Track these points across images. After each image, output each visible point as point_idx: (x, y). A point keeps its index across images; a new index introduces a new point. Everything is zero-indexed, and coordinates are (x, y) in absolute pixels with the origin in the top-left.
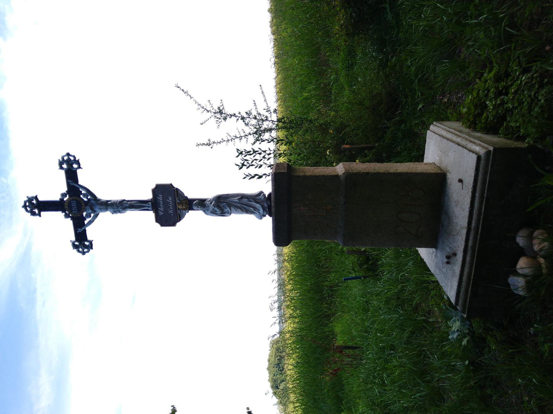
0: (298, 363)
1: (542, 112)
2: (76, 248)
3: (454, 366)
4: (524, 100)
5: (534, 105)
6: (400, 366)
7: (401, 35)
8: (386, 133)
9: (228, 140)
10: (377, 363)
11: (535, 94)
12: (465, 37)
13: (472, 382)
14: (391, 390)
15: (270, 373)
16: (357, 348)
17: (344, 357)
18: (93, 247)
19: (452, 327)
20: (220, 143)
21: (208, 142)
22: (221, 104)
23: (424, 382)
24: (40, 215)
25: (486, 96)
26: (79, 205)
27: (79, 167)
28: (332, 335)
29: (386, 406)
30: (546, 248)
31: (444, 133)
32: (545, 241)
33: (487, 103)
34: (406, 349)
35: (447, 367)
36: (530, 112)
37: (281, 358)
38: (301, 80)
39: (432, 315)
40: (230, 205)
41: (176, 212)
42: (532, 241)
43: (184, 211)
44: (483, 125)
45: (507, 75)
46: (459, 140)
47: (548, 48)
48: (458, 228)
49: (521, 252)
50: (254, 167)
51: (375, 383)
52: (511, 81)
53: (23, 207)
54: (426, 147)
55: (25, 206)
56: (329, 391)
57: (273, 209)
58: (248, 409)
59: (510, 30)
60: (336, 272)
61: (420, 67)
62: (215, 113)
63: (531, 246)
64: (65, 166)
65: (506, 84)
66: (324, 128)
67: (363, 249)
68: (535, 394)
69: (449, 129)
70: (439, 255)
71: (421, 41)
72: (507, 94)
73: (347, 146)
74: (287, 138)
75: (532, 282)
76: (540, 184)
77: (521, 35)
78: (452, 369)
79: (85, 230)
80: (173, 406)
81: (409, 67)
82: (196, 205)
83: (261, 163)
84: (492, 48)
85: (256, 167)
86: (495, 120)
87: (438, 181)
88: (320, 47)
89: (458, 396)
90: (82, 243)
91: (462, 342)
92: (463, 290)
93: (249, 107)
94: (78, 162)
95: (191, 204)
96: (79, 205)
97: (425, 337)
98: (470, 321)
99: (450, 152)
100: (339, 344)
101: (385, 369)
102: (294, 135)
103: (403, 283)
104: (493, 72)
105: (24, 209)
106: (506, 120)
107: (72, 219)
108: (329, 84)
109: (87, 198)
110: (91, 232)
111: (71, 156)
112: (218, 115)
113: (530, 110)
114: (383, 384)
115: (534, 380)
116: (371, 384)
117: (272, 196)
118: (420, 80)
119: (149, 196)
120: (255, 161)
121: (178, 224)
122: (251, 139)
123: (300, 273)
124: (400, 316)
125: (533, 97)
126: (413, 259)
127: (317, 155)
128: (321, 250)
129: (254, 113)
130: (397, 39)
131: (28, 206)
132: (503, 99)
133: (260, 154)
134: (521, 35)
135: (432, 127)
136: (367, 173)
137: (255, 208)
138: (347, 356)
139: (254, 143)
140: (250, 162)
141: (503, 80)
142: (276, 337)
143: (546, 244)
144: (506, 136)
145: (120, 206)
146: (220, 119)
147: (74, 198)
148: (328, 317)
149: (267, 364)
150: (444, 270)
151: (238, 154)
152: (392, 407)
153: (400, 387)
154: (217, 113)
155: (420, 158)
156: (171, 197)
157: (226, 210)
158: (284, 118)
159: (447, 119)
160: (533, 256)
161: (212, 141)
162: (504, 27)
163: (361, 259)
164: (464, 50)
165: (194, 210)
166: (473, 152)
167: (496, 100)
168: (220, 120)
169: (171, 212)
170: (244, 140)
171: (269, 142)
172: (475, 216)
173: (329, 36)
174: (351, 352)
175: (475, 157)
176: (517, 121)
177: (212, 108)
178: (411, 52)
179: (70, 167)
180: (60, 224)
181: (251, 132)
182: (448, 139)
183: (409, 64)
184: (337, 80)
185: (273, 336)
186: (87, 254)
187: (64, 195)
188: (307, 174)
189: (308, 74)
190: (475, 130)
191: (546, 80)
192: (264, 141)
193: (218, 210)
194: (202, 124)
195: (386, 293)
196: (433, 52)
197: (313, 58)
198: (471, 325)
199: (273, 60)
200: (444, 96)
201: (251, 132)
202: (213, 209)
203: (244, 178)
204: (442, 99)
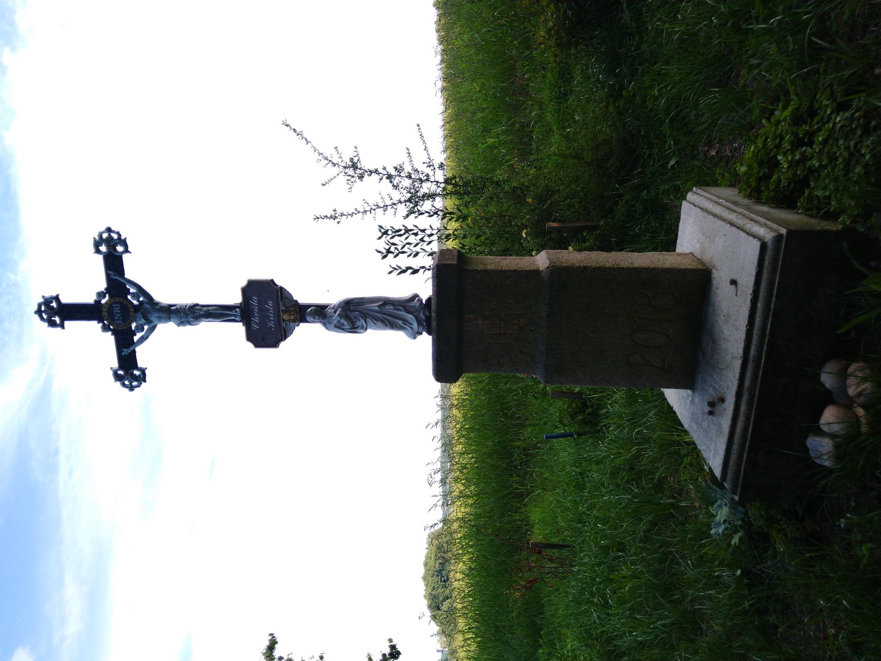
0: (470, 569)
1: (866, 173)
2: (119, 380)
3: (718, 577)
4: (838, 154)
5: (853, 162)
6: (634, 576)
7: (644, 47)
9: (365, 212)
10: (596, 572)
11: (856, 145)
12: (747, 51)
13: (746, 604)
14: (618, 614)
15: (427, 586)
16: (565, 546)
19: (715, 516)
20: (352, 215)
22: (355, 154)
24: (63, 327)
25: (778, 147)
26: (124, 311)
27: (126, 251)
28: (526, 525)
31: (709, 206)
32: (866, 381)
33: (780, 158)
35: (708, 579)
36: (846, 174)
37: (445, 562)
38: (483, 117)
43: (292, 324)
44: (772, 194)
46: (732, 217)
48: (729, 358)
49: (827, 398)
50: (406, 255)
51: (592, 603)
52: (817, 123)
53: (36, 312)
54: (681, 228)
55: (39, 312)
56: (519, 614)
57: (434, 324)
58: (390, 640)
59: (819, 42)
60: (535, 425)
61: (673, 98)
62: (345, 167)
63: (844, 388)
64: (103, 248)
65: (810, 127)
66: (518, 195)
67: (577, 390)
68: (846, 624)
70: (697, 400)
72: (810, 144)
73: (554, 225)
74: (459, 210)
75: (845, 445)
78: (716, 583)
79: (134, 352)
80: (271, 635)
81: (656, 99)
82: (311, 314)
83: (418, 249)
84: (788, 70)
86: (792, 186)
87: (698, 281)
90: (129, 371)
92: (733, 457)
93: (400, 158)
94: (124, 243)
95: (303, 313)
96: (124, 311)
98: (744, 507)
99: (718, 236)
101: (608, 581)
103: (639, 444)
104: (790, 109)
105: (37, 317)
106: (808, 186)
107: (115, 333)
108: (528, 125)
109: (138, 301)
110: (144, 355)
111: (114, 232)
112: (351, 172)
113: (847, 170)
115: (845, 602)
116: (585, 604)
117: (433, 302)
118: (672, 120)
119: (235, 298)
120: (407, 246)
121: (282, 344)
122: (403, 209)
123: (477, 427)
124: (634, 497)
125: (852, 150)
129: (408, 168)
130: (638, 54)
131: (44, 311)
132: (805, 152)
133: (416, 234)
135: (690, 196)
136: (585, 267)
137: (405, 321)
138: (549, 559)
139: (407, 216)
140: (399, 247)
141: (805, 122)
143: (867, 385)
144: (807, 211)
146: (353, 177)
147: (117, 299)
148: (520, 496)
149: (422, 571)
151: (380, 234)
152: (619, 642)
154: (349, 167)
155: (670, 245)
157: (358, 323)
158: (454, 177)
159: (715, 183)
160: (847, 404)
161: (339, 211)
162: (810, 35)
164: (744, 72)
166: (755, 237)
167: (793, 153)
168: (353, 180)
169: (271, 324)
170: (390, 211)
171: (430, 216)
174: (556, 553)
175: (757, 244)
179: (112, 250)
180: (95, 342)
181: (403, 199)
182: (715, 215)
183: (657, 94)
184: (541, 118)
187: (101, 295)
189: (494, 109)
190: (758, 201)
191: (874, 123)
192: (422, 214)
193: (345, 323)
194: (323, 185)
198: (746, 513)
199: (440, 84)
200: (711, 147)
201: (403, 199)
202: (338, 322)
203: (390, 273)
204: (708, 151)
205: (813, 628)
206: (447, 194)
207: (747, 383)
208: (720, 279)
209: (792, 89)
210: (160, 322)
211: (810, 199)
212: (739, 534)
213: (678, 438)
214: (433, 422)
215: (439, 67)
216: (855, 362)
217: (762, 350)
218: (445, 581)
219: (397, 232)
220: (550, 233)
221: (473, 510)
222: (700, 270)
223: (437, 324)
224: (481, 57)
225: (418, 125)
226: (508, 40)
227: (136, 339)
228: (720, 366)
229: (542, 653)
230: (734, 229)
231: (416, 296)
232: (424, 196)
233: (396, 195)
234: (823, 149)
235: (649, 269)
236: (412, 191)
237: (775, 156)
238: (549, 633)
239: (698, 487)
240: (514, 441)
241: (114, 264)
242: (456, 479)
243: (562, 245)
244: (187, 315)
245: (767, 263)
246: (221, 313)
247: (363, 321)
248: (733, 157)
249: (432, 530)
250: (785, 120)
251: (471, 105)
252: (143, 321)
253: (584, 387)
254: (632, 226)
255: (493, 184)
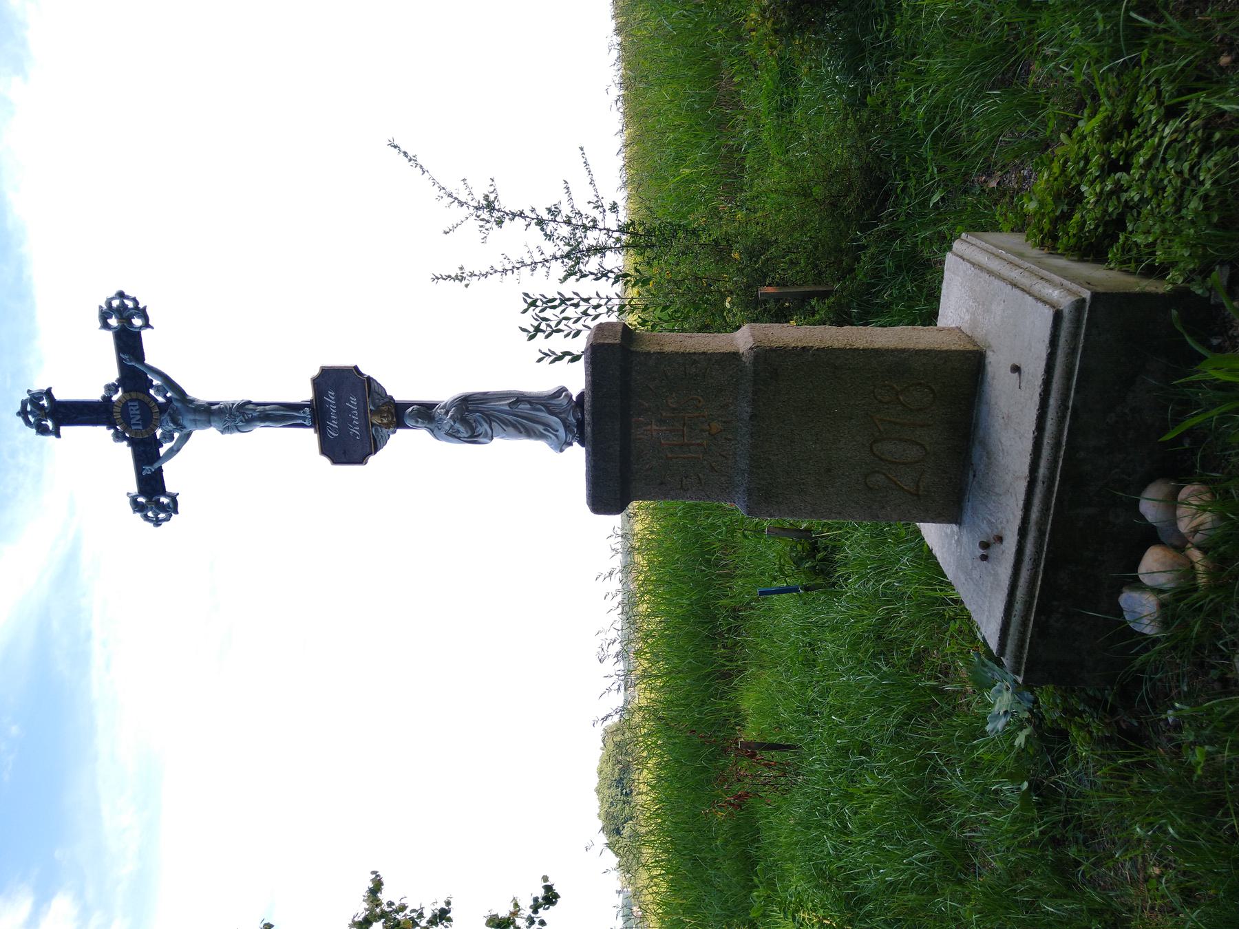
0: (659, 778)
1: (1205, 209)
2: (140, 511)
3: (996, 792)
4: (1166, 182)
5: (1187, 193)
6: (880, 791)
7: (897, 32)
8: (858, 259)
9: (505, 271)
10: (830, 783)
11: (1191, 169)
12: (1039, 35)
13: (1036, 831)
14: (860, 843)
15: (602, 800)
16: (789, 747)
17: (759, 767)
18: (179, 509)
19: (992, 706)
20: (486, 275)
21: (459, 273)
22: (492, 189)
23: (930, 826)
24: (58, 435)
25: (1082, 173)
26: (145, 412)
27: (147, 325)
28: (736, 717)
29: (848, 879)
30: (1207, 526)
31: (984, 259)
32: (1205, 511)
33: (1084, 188)
34: (895, 752)
35: (982, 794)
36: (1179, 210)
37: (626, 769)
38: (675, 139)
39: (952, 676)
40: (489, 419)
41: (368, 431)
42: (1175, 508)
43: (385, 430)
44: (1072, 241)
45: (1130, 123)
46: (1015, 274)
47: (1224, 60)
48: (1009, 478)
49: (1150, 536)
50: (562, 334)
51: (825, 827)
52: (1138, 137)
53: (19, 414)
54: (943, 292)
55: (23, 413)
56: (726, 842)
57: (588, 430)
58: (545, 879)
59: (1141, 18)
60: (747, 576)
61: (936, 107)
62: (477, 208)
63: (1173, 522)
64: (113, 322)
65: (1127, 144)
66: (720, 250)
67: (804, 526)
68: (1175, 861)
69: (994, 250)
70: (965, 539)
71: (941, 46)
72: (1127, 168)
73: (770, 290)
74: (637, 271)
75: (1175, 606)
76: (1194, 378)
77: (1165, 31)
78: (993, 800)
79: (160, 470)
80: (373, 873)
81: (913, 107)
82: (411, 415)
83: (579, 326)
84: (1098, 61)
85: (566, 336)
86: (1100, 230)
87: (966, 371)
88: (719, 64)
89: (1004, 860)
90: (153, 498)
91: (1014, 738)
92: (1015, 621)
93: (555, 196)
94: (143, 314)
95: (400, 415)
96: (145, 412)
97: (936, 726)
98: (1032, 692)
99: (996, 302)
100: (749, 739)
101: (848, 796)
102: (656, 261)
103: (889, 602)
104: (1099, 117)
105: (20, 420)
106: (1124, 229)
107: (133, 443)
108: (738, 150)
109: (165, 396)
110: (174, 474)
111: (128, 298)
112: (485, 214)
113: (1179, 204)
114: (844, 831)
115: (1171, 830)
116: (816, 829)
117: (587, 398)
118: (936, 138)
119: (305, 394)
120: (564, 322)
121: (372, 459)
122: (558, 269)
123: (666, 578)
124: (882, 678)
125: (1186, 176)
126: (912, 549)
127: (705, 310)
128: (714, 527)
129: (566, 210)
130: (889, 44)
131: (31, 412)
132: (1119, 180)
133: (576, 305)
134: (1165, 31)
135: (956, 245)
136: (804, 348)
137: (547, 426)
138: (765, 765)
139: (565, 278)
140: (553, 324)
141: (1121, 136)
142: (609, 722)
143: (1207, 518)
144: (1124, 264)
145: (240, 416)
146: (488, 222)
147: (134, 395)
148: (727, 676)
149: (595, 780)
150: (976, 574)
151: (526, 306)
152: (861, 883)
153: (880, 837)
154: (483, 208)
155: (930, 318)
156: (356, 396)
157: (480, 430)
158: (633, 223)
159: (995, 227)
160: (1179, 546)
161: (467, 271)
162: (1127, 10)
163: (799, 547)
164: (1035, 67)
165: (407, 427)
166: (1045, 302)
167: (1102, 182)
168: (488, 226)
169: (355, 430)
170: (541, 270)
171: (597, 279)
172: (1046, 452)
173: (739, 38)
174: (775, 756)
175: (1048, 313)
176: (1148, 232)
177: (470, 198)
178: (919, 72)
179: (126, 324)
180: (102, 455)
181: (558, 254)
182: (990, 273)
183: (913, 100)
184: (755, 139)
185: (605, 719)
186: (164, 524)
187: (111, 388)
188: (668, 349)
189: (691, 126)
190: (1053, 251)
191: (1217, 136)
192: (585, 276)
193: (462, 429)
194: (446, 233)
195: (852, 625)
196: (968, 71)
197: (702, 88)
198: (1035, 702)
199: (616, 92)
200: (989, 176)
201: (558, 254)
203: (540, 360)
204: (985, 181)
205: (1128, 865)
206: (623, 247)
207: (1035, 515)
208: (997, 365)
209: (1100, 88)
210: (197, 428)
211: (1126, 249)
212: (1026, 732)
213: (942, 594)
214: (606, 572)
215: (616, 68)
216: (1189, 483)
217: (1056, 467)
218: (627, 794)
219: (549, 303)
220: (765, 302)
221: (661, 696)
222: (970, 352)
223: (593, 430)
224: (671, 53)
225: (582, 149)
226: (711, 27)
227: (162, 451)
228: (997, 490)
229: (758, 897)
230: (1017, 292)
231: (563, 390)
232: (588, 250)
233: (549, 249)
234: (1145, 175)
235: (895, 350)
236: (572, 242)
237: (1078, 186)
238: (767, 869)
239: (969, 663)
240: (719, 598)
241: (129, 345)
242: (638, 653)
243: (781, 317)
244: (234, 418)
245: (1062, 342)
246: (282, 414)
247: (486, 426)
248: (1021, 189)
249: (606, 723)
250: (1092, 133)
251: (659, 121)
252: (171, 426)
253: (814, 521)
254: (880, 291)
255: (683, 228)
